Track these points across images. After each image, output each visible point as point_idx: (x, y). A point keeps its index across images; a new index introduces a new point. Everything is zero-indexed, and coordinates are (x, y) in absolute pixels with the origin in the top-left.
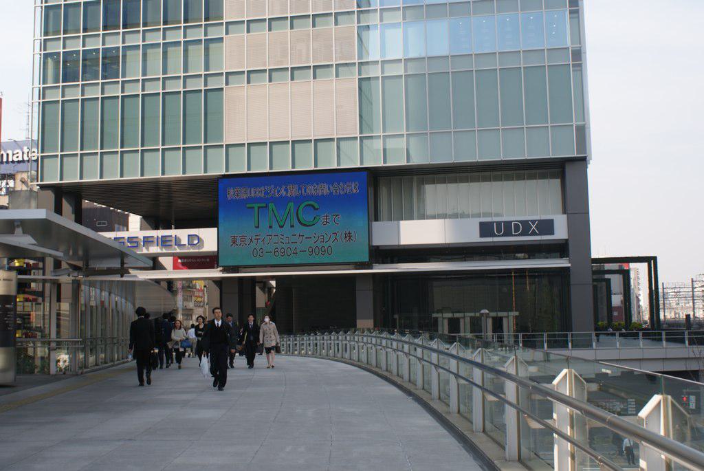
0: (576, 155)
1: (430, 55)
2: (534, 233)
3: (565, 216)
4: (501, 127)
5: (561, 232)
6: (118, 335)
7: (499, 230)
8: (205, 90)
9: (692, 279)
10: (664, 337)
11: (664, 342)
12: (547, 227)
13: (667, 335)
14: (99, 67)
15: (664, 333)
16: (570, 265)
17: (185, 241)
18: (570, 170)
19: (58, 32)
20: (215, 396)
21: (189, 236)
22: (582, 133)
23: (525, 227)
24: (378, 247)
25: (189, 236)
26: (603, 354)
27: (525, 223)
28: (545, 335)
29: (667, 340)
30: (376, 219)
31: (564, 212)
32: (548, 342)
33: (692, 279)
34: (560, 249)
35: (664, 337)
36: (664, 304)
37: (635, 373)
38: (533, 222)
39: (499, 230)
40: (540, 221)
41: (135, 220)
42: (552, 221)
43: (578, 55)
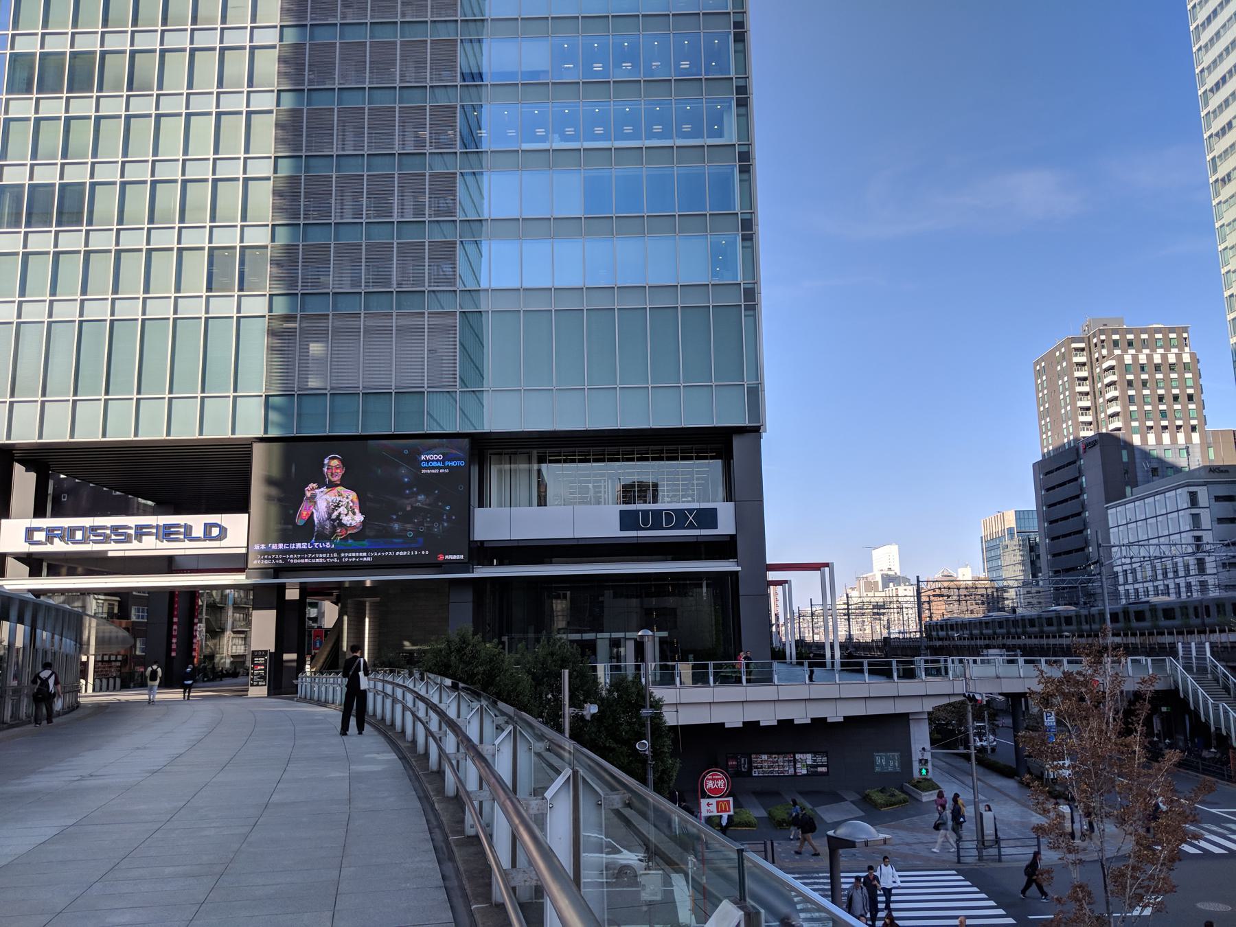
0: (747, 424)
1: (557, 286)
2: (691, 526)
3: (732, 504)
4: (650, 386)
5: (726, 525)
6: (101, 681)
7: (645, 522)
8: (237, 317)
9: (918, 577)
10: (866, 667)
11: (867, 675)
12: (708, 517)
13: (870, 664)
14: (7, 228)
15: (866, 662)
16: (739, 569)
17: (198, 531)
18: (738, 443)
19: (18, 225)
20: (340, 739)
21: (205, 524)
22: (755, 394)
23: (681, 518)
24: (482, 542)
25: (205, 524)
26: (787, 692)
27: (681, 513)
28: (894, 662)
29: (871, 672)
30: (481, 505)
31: (729, 497)
32: (715, 674)
33: (918, 577)
34: (724, 548)
35: (866, 667)
36: (800, 628)
37: (347, 585)
38: (691, 511)
39: (645, 522)
40: (700, 511)
41: (368, 584)
42: (713, 512)
43: (751, 294)
